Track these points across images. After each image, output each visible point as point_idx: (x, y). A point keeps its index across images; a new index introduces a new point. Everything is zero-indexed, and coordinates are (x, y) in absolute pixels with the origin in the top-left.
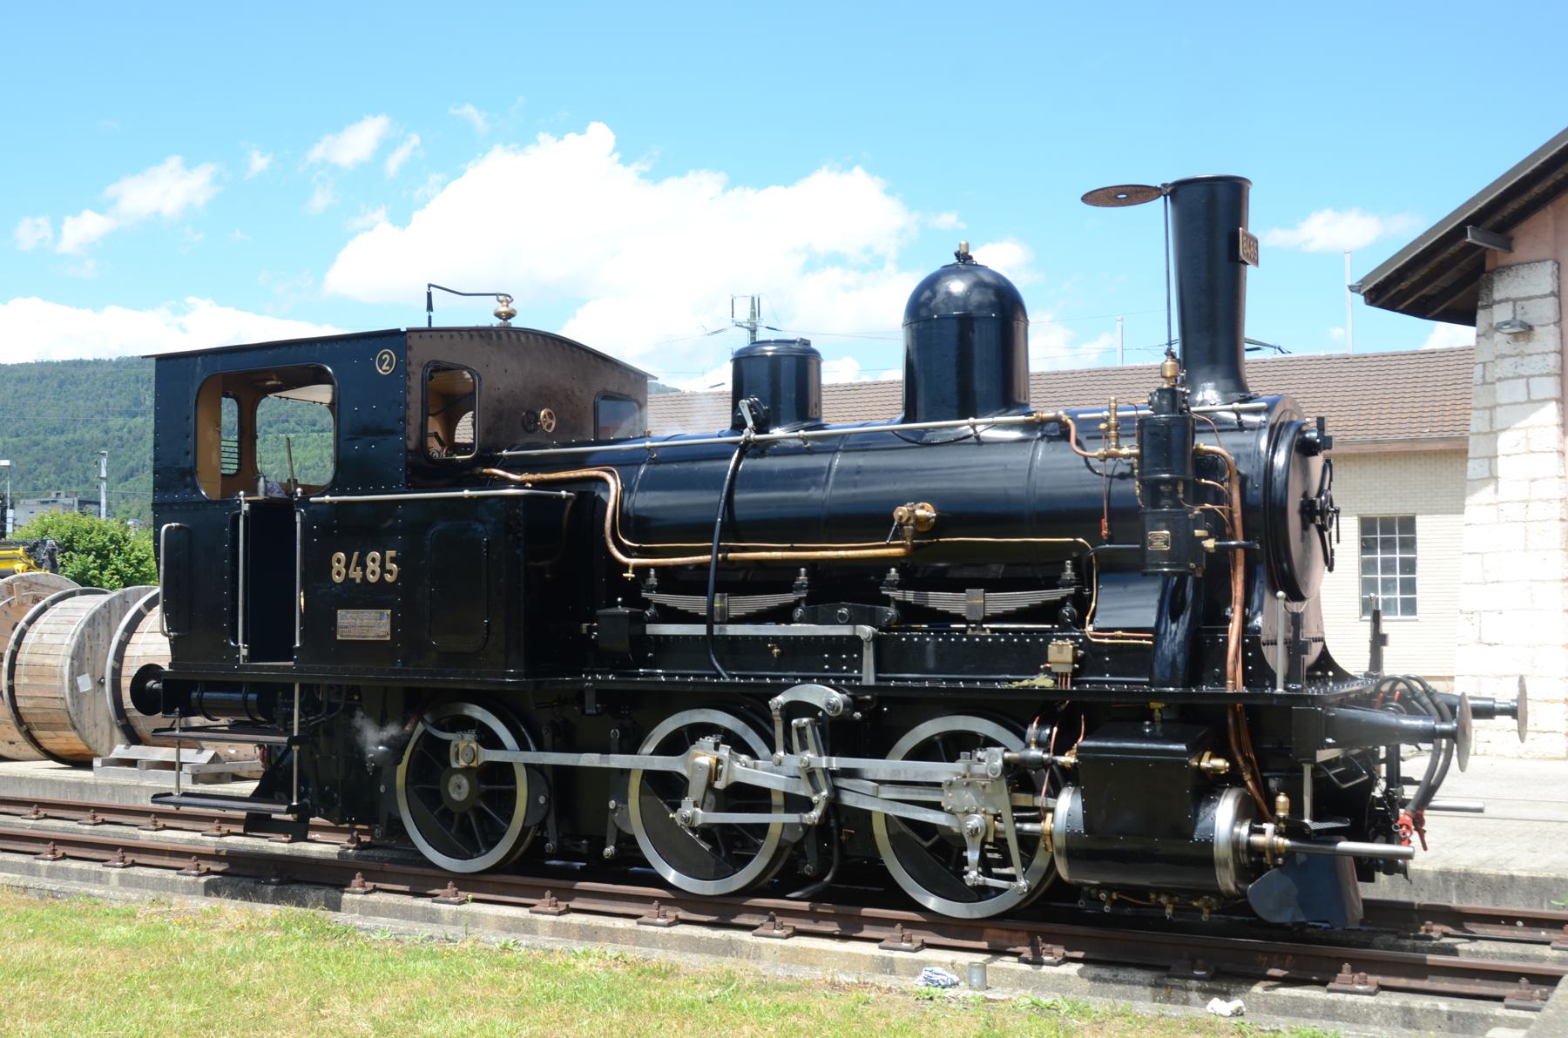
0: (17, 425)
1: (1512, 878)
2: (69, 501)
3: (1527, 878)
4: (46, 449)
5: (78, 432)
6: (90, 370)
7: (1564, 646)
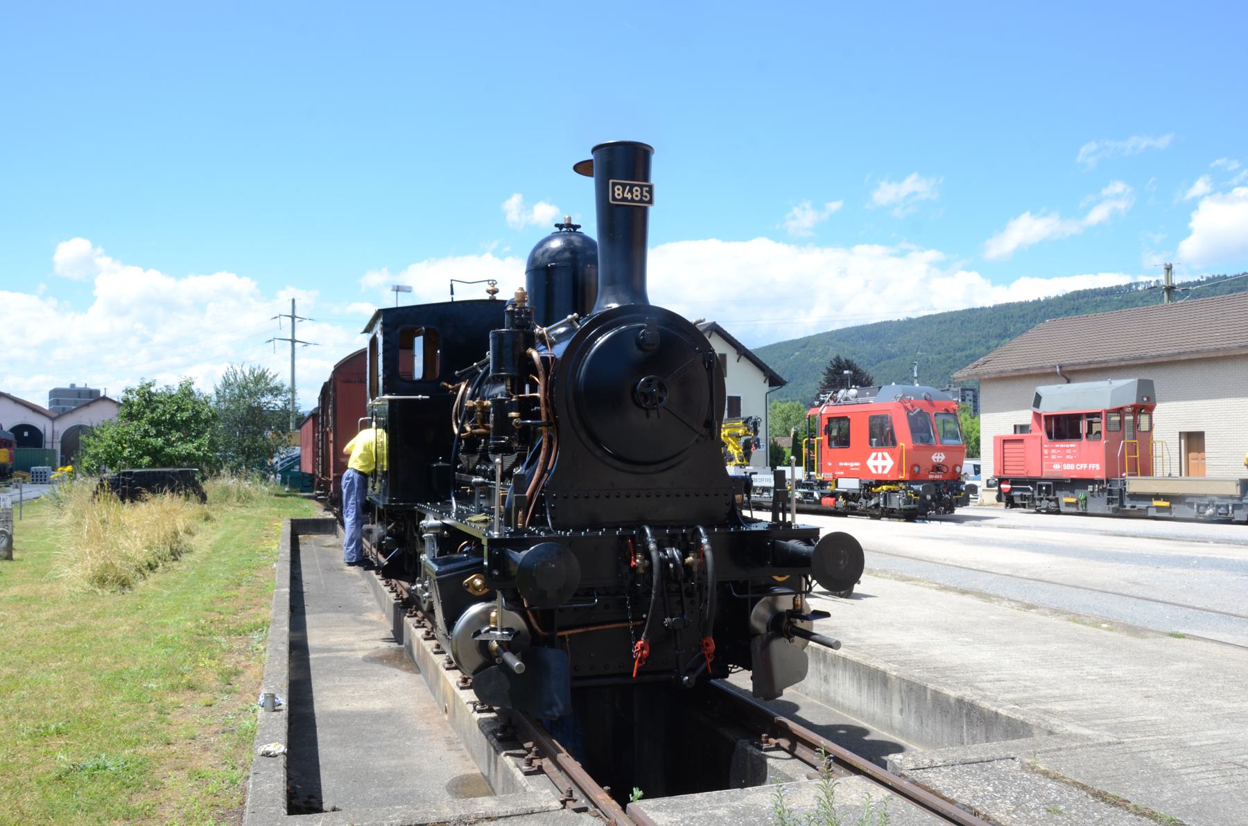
1: (996, 713)
2: (956, 389)
3: (1006, 717)
4: (954, 360)
5: (972, 350)
6: (978, 314)
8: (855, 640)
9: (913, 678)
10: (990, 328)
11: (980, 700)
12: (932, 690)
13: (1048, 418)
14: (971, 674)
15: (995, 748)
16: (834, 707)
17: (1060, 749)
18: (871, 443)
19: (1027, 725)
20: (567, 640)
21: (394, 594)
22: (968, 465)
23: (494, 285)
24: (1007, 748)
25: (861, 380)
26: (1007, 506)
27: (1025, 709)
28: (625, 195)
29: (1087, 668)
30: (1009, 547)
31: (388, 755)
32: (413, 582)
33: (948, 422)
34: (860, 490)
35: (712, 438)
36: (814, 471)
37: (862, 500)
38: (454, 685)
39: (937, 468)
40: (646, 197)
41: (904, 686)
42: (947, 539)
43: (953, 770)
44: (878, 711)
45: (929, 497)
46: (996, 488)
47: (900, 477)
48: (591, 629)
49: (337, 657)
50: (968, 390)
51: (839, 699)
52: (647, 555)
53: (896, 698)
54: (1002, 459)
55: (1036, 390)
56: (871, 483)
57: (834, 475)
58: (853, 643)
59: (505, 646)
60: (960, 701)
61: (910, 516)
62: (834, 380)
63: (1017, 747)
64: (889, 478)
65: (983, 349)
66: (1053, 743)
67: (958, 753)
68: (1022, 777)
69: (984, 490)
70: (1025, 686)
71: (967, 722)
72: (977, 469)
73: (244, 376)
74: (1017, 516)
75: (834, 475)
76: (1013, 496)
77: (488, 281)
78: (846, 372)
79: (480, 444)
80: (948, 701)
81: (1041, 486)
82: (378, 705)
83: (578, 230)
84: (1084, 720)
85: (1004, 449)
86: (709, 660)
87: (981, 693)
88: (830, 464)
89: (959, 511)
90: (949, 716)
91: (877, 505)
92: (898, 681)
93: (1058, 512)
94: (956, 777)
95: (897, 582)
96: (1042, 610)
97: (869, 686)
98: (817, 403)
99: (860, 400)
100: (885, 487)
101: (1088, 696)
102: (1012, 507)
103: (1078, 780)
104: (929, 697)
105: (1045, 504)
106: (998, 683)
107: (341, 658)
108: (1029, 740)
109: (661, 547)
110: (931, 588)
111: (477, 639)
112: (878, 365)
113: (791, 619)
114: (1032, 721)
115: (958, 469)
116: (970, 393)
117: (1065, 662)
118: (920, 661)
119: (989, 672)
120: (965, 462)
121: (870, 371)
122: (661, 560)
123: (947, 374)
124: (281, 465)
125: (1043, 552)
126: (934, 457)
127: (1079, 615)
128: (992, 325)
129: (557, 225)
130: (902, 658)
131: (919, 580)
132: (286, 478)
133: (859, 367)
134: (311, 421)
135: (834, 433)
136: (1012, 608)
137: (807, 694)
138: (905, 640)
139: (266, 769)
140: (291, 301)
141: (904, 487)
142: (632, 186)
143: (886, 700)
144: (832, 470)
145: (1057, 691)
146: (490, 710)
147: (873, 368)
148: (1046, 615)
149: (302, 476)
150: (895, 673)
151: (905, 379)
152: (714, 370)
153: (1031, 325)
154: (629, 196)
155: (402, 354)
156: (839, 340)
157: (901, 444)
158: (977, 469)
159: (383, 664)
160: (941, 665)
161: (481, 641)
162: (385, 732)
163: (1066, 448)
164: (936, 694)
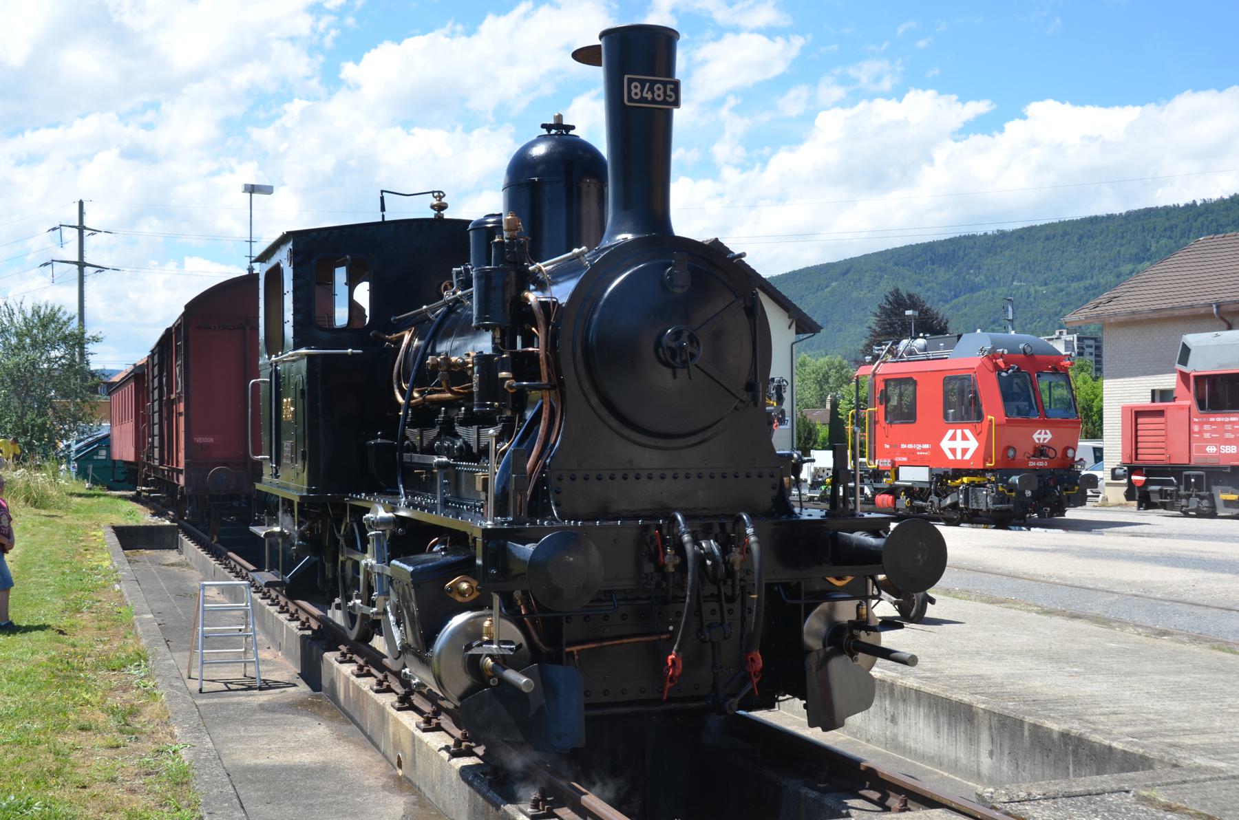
0: (1046, 275)
1: (1110, 748)
2: (1070, 338)
3: (1122, 751)
4: (1068, 294)
5: (1095, 279)
7: (113, 527)
8: (931, 670)
9: (1006, 711)
10: (1122, 245)
11: (1091, 733)
12: (1030, 724)
13: (1200, 379)
14: (1080, 707)
15: (1107, 780)
16: (903, 754)
17: (1185, 782)
18: (946, 416)
19: (1147, 759)
20: (576, 657)
21: (298, 623)
22: (1085, 447)
23: (441, 198)
24: (1122, 780)
25: (931, 326)
26: (1140, 506)
27: (1146, 742)
28: (645, 95)
29: (1229, 700)
30: (1140, 560)
31: (337, 813)
32: (325, 604)
33: (1058, 386)
34: (930, 483)
35: (756, 404)
36: (864, 457)
37: (933, 498)
38: (412, 728)
39: (1040, 451)
40: (671, 97)
41: (995, 721)
42: (1054, 551)
43: (1055, 803)
44: (962, 755)
45: (1028, 493)
46: (1125, 481)
47: (988, 465)
48: (605, 644)
49: (233, 703)
50: (1088, 338)
51: (911, 744)
52: (680, 549)
53: (985, 736)
54: (1134, 439)
55: (1183, 340)
56: (946, 473)
57: (893, 463)
58: (928, 674)
59: (501, 662)
60: (1065, 735)
61: (1001, 520)
62: (891, 325)
63: (1133, 779)
64: (972, 466)
65: (1111, 278)
66: (1177, 776)
67: (1060, 786)
68: (1137, 810)
69: (1108, 484)
70: (1148, 720)
71: (1074, 761)
72: (1098, 454)
73: (25, 319)
74: (1157, 519)
75: (893, 463)
76: (1148, 492)
77: (433, 192)
78: (908, 313)
79: (440, 413)
80: (1050, 737)
81: (1188, 477)
82: (306, 758)
83: (571, 132)
84: (1218, 753)
85: (1136, 424)
86: (756, 680)
87: (1093, 726)
88: (887, 446)
89: (1071, 514)
90: (1052, 756)
91: (954, 506)
92: (987, 716)
93: (1212, 515)
94: (1058, 809)
95: (984, 604)
96: (1178, 637)
97: (950, 724)
98: (868, 358)
99: (931, 354)
100: (965, 480)
101: (1225, 730)
102: (1146, 508)
103: (1203, 811)
104: (1026, 733)
105: (1194, 502)
106: (1114, 717)
107: (239, 704)
108: (1148, 773)
109: (696, 541)
110: (1029, 611)
111: (470, 653)
112: (955, 301)
113: (855, 632)
114: (1154, 754)
115: (1070, 453)
116: (1091, 342)
117: (1202, 694)
118: (1015, 694)
119: (1103, 704)
120: (1080, 443)
121: (943, 310)
122: (697, 555)
123: (1056, 314)
124: (78, 451)
125: (1186, 567)
126: (1036, 436)
127: (1227, 643)
128: (1124, 241)
129: (544, 126)
130: (991, 690)
131: (1014, 602)
132: (86, 469)
133: (928, 305)
134: (131, 386)
135: (894, 402)
136: (1139, 634)
137: (868, 741)
138: (996, 670)
139: (220, 809)
140: (77, 206)
141: (993, 479)
142: (653, 83)
143: (973, 740)
144: (887, 454)
145: (1187, 724)
146: (469, 753)
147: (947, 306)
148: (1183, 642)
149: (113, 464)
150: (983, 706)
151: (994, 322)
152: (757, 318)
153: (1182, 241)
154: (649, 96)
155: (319, 292)
156: (896, 264)
157: (989, 417)
158: (1098, 455)
159: (298, 711)
160: (1042, 698)
161: (471, 655)
162: (324, 788)
163: (1225, 423)
164: (1035, 728)
